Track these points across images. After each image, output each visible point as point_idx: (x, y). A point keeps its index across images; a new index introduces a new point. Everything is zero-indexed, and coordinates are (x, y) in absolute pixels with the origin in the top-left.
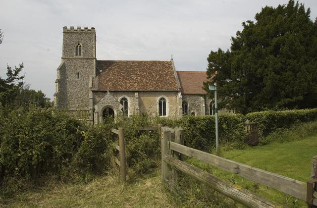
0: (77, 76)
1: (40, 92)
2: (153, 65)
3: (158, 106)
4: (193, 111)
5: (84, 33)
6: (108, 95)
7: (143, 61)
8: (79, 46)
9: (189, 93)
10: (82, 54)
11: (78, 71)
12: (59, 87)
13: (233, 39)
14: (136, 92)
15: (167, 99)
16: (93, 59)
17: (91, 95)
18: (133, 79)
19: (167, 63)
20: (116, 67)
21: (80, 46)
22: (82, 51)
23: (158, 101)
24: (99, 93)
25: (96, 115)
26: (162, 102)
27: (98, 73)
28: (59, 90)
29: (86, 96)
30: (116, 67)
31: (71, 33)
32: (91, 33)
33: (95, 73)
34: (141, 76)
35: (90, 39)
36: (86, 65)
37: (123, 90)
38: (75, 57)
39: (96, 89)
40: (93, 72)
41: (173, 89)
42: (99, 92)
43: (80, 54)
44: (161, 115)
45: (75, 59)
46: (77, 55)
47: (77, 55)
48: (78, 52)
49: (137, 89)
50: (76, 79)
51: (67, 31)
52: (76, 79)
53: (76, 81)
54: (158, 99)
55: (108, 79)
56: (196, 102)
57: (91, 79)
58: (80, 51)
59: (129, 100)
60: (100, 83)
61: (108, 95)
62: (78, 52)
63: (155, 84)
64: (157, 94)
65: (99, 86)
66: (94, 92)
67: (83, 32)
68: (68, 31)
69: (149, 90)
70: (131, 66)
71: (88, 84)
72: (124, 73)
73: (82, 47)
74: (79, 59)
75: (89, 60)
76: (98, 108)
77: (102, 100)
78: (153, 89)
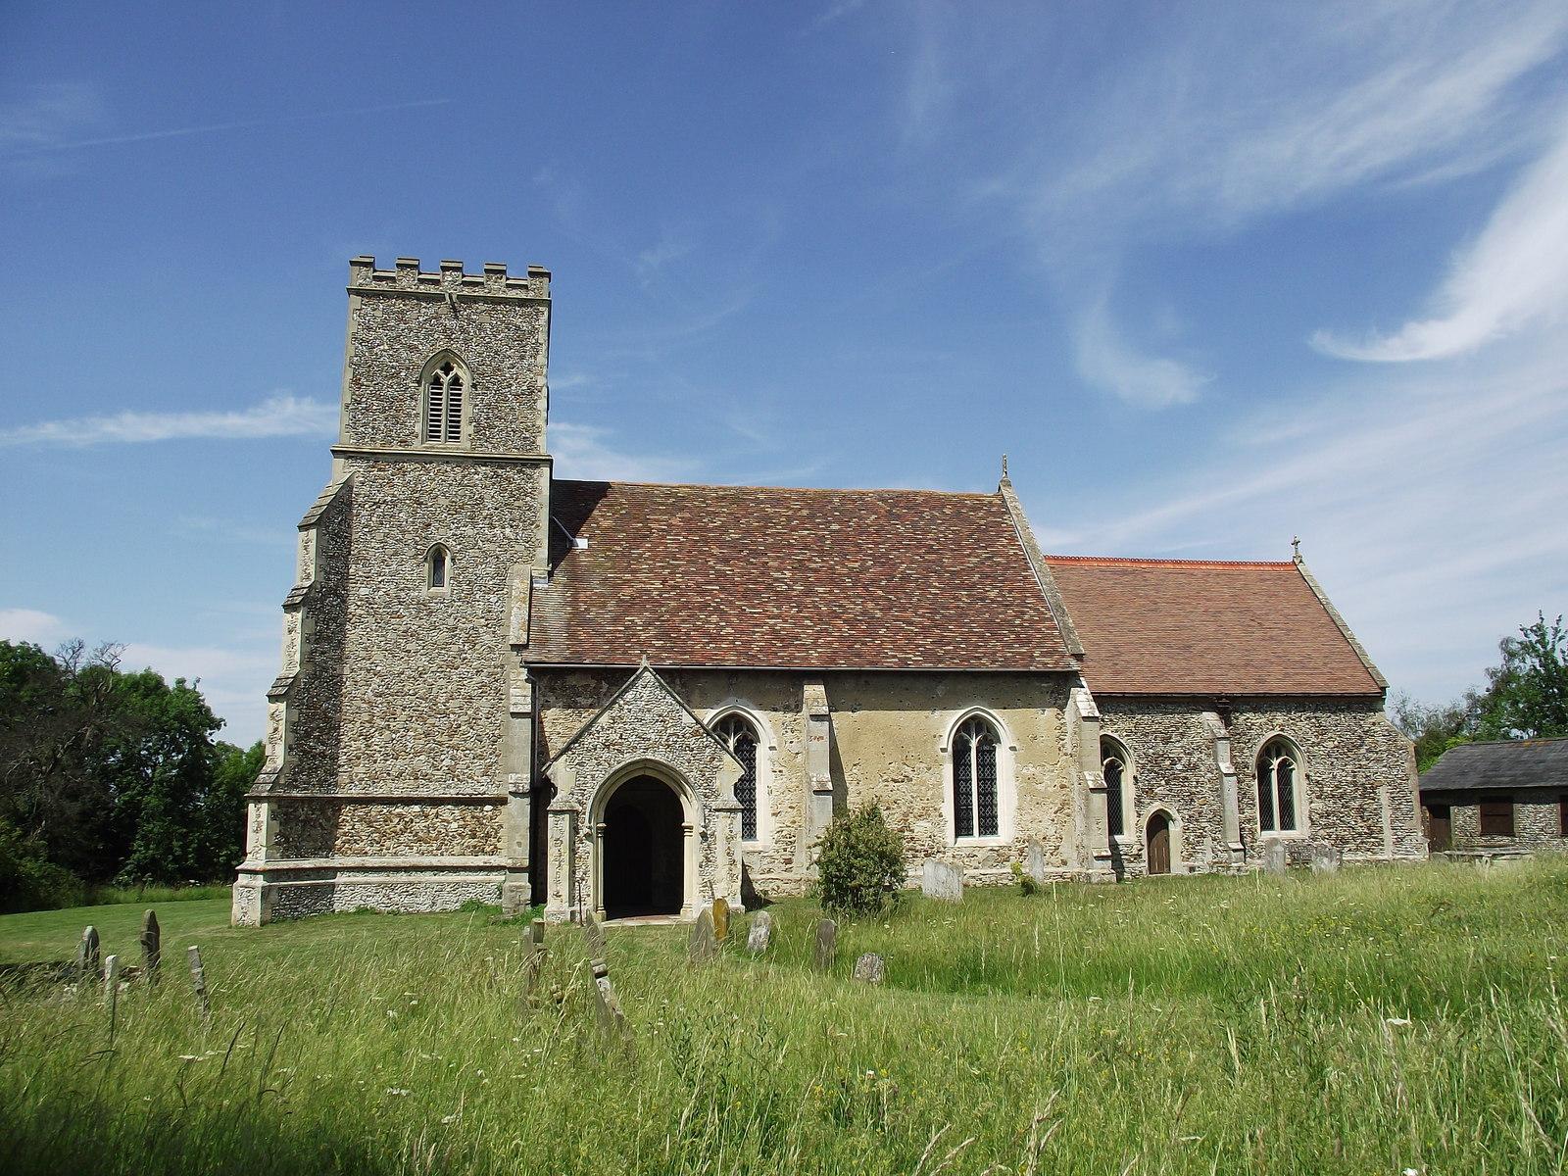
0: (426, 569)
1: (161, 677)
2: (898, 517)
3: (948, 769)
4: (1156, 806)
5: (485, 300)
6: (646, 696)
7: (835, 493)
8: (446, 379)
9: (987, 665)
10: (466, 429)
11: (438, 535)
12: (306, 640)
13: (216, 724)
14: (814, 676)
15: (1003, 720)
16: (536, 463)
17: (520, 694)
18: (783, 598)
19: (978, 504)
20: (675, 521)
21: (456, 381)
22: (467, 411)
23: (946, 742)
24: (572, 681)
25: (557, 828)
26: (974, 743)
27: (560, 548)
28: (308, 658)
29: (484, 705)
30: (675, 521)
31: (403, 296)
32: (523, 303)
33: (543, 552)
34: (833, 580)
35: (521, 337)
36: (491, 497)
37: (731, 662)
38: (417, 446)
39: (554, 655)
40: (531, 545)
41: (1042, 662)
42: (573, 681)
43: (454, 433)
44: (969, 833)
45: (424, 459)
46: (433, 434)
47: (433, 434)
48: (444, 420)
49: (815, 661)
50: (425, 592)
51: (374, 286)
52: (425, 592)
53: (422, 604)
54: (947, 722)
55: (626, 593)
56: (1175, 749)
57: (519, 594)
58: (455, 410)
59: (765, 722)
60: (577, 620)
61: (646, 696)
62: (444, 420)
63: (925, 631)
64: (940, 690)
65: (572, 636)
66: (539, 675)
67: (479, 292)
68: (384, 286)
69: (890, 663)
70: (768, 518)
71: (496, 622)
72: (726, 561)
73: (466, 389)
74: (447, 459)
75: (511, 473)
76: (576, 783)
77: (604, 720)
78: (916, 662)
